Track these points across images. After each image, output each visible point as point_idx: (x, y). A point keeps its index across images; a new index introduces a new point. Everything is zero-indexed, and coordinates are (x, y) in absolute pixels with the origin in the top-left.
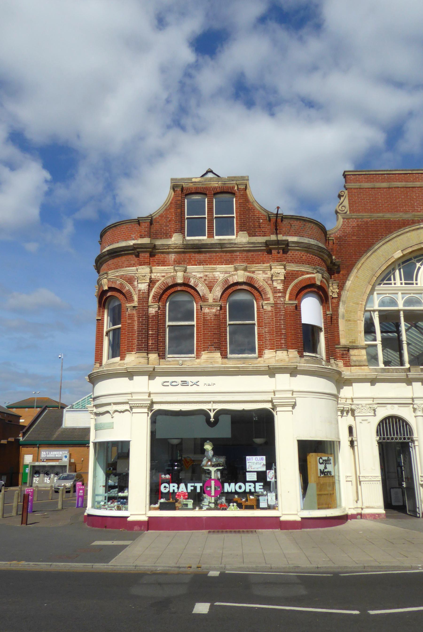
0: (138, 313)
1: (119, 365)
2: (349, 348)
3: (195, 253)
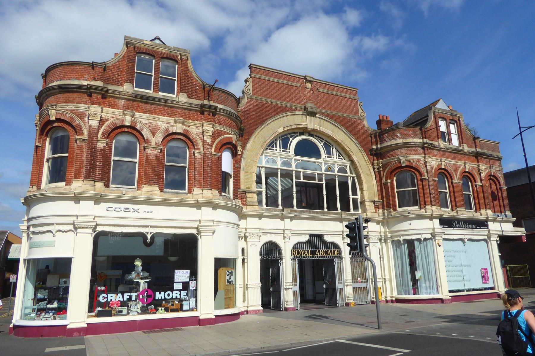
0: (88, 146)
1: (64, 190)
2: (246, 192)
3: (142, 103)
